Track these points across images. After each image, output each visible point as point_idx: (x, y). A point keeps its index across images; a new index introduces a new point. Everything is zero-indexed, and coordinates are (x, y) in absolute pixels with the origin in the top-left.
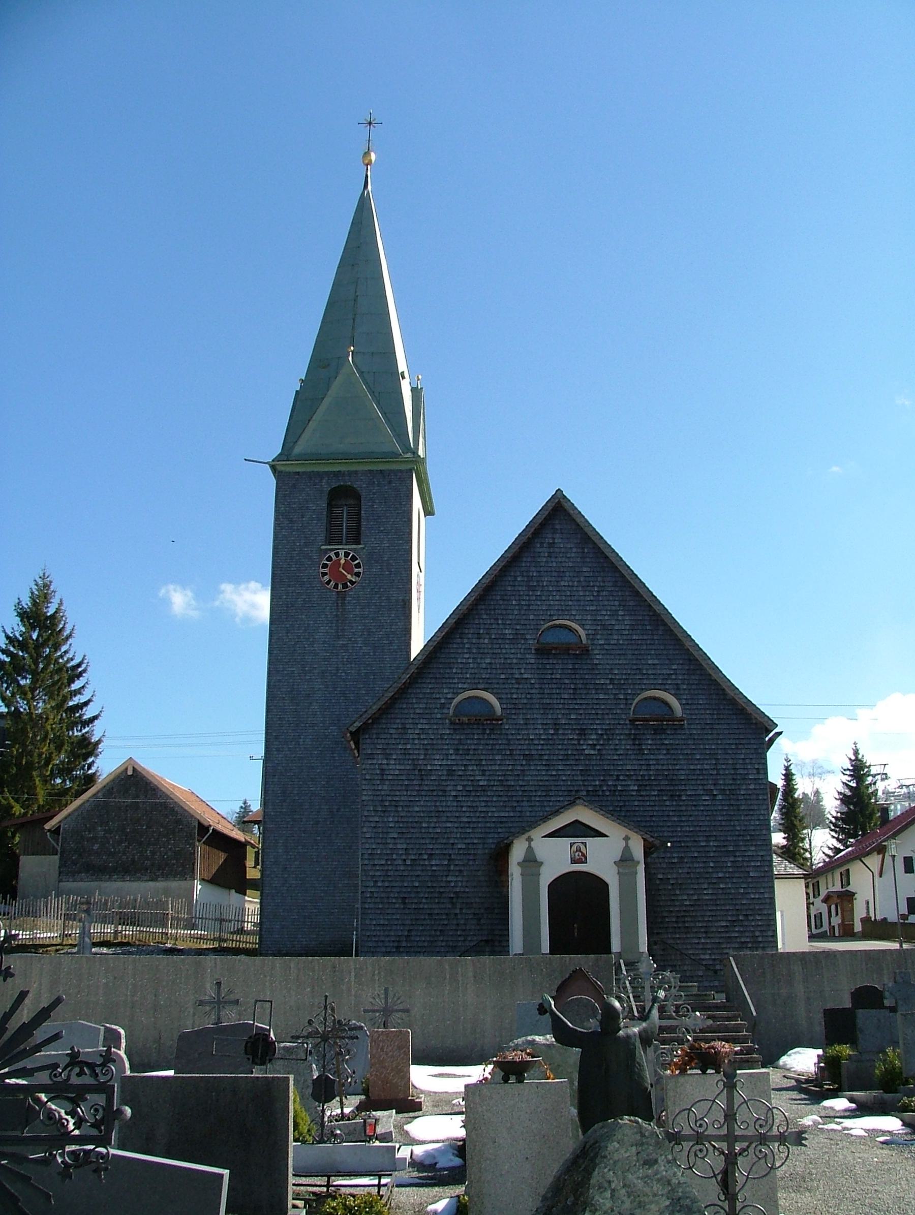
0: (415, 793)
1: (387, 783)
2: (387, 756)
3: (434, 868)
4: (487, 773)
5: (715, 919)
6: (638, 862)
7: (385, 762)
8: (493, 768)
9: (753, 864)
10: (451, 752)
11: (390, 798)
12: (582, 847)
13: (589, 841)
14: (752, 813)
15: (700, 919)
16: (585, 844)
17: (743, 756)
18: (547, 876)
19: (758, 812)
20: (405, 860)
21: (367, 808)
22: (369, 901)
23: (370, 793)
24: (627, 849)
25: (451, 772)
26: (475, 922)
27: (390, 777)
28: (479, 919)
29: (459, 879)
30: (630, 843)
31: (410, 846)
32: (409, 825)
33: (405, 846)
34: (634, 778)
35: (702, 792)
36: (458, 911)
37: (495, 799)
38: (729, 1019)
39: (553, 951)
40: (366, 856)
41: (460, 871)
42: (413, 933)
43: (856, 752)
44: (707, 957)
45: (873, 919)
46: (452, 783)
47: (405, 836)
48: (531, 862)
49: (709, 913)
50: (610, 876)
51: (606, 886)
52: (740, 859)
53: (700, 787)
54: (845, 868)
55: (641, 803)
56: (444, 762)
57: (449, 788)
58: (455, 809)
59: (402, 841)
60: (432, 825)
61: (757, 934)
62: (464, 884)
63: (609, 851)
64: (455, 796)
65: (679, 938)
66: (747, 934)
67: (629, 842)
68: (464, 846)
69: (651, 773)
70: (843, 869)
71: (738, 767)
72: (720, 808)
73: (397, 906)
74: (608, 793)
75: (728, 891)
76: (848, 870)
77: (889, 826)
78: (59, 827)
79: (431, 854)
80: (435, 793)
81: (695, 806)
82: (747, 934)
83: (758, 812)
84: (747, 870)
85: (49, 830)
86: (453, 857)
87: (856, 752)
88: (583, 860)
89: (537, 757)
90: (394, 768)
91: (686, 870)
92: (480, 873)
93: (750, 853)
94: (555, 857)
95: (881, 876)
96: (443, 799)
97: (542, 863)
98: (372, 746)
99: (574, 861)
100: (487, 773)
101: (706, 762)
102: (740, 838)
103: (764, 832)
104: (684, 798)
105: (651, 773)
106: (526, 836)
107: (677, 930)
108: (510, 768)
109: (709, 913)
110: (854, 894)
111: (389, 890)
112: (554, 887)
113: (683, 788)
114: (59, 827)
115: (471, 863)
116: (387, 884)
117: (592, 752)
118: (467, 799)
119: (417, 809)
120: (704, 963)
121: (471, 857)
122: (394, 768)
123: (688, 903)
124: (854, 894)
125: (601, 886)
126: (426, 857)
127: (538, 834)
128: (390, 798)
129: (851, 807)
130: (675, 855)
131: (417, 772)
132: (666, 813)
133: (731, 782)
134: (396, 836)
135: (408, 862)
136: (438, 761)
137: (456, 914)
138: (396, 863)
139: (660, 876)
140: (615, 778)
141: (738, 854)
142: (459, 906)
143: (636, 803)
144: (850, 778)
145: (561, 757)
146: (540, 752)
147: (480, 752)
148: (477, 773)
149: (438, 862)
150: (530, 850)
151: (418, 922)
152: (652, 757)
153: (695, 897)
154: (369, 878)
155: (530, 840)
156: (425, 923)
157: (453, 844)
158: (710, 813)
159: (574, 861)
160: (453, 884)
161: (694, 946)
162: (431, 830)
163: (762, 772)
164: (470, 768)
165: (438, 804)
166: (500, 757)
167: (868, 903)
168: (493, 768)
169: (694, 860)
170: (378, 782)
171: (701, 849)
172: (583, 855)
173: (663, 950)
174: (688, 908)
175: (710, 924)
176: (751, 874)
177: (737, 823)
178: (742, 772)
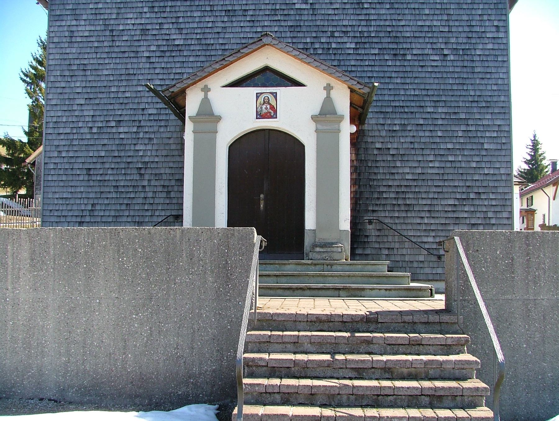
0: (105, 56)
1: (76, 45)
2: (76, 17)
3: (122, 136)
4: (184, 31)
5: (441, 196)
6: (342, 117)
7: (74, 23)
8: (191, 25)
9: (488, 134)
10: (146, 10)
11: (78, 62)
12: (271, 98)
13: (281, 91)
14: (488, 76)
15: (424, 196)
16: (275, 95)
17: (480, 12)
18: (227, 135)
19: (496, 76)
20: (91, 128)
21: (55, 73)
22: (52, 172)
23: (58, 57)
24: (328, 101)
25: (144, 31)
26: (164, 195)
27: (79, 39)
28: (169, 192)
29: (149, 147)
30: (333, 94)
31: (98, 113)
32: (98, 90)
33: (92, 113)
34: (351, 34)
35: (430, 52)
36: (145, 183)
37: (191, 59)
38: (448, 349)
39: (230, 223)
40: (51, 125)
41: (150, 139)
42: (98, 207)
43: (535, 137)
44: (430, 239)
45: (547, 225)
46: (146, 43)
47: (92, 102)
48: (209, 117)
49: (434, 190)
50: (307, 136)
51: (302, 147)
52: (473, 128)
53: (429, 46)
54: (530, 195)
55: (359, 63)
56: (138, 21)
57: (143, 49)
58: (147, 71)
59: (89, 107)
60: (122, 89)
61: (490, 215)
62: (154, 153)
63: (308, 106)
64: (149, 57)
65: (398, 217)
66: (478, 215)
67: (332, 92)
68: (155, 112)
69: (372, 29)
70: (529, 196)
71: (474, 23)
72: (451, 70)
73: (81, 178)
74: (320, 52)
75: (458, 165)
76: (532, 196)
77: (556, 172)
78: (35, 162)
79: (120, 121)
80: (126, 55)
81: (422, 66)
82: (478, 215)
83: (496, 76)
84: (481, 141)
85: (29, 163)
86: (143, 124)
87: (535, 137)
88: (272, 113)
89: (240, 13)
90: (84, 29)
91: (409, 140)
92: (171, 141)
93: (485, 122)
94: (230, 109)
95: (554, 200)
96: (135, 60)
97: (219, 118)
98: (61, 7)
99: (260, 116)
100: (184, 31)
101: (436, 18)
102: (474, 105)
103: (502, 98)
104: (409, 57)
105: (372, 29)
106: (201, 85)
107: (396, 208)
108: (210, 25)
109: (434, 190)
110: (535, 211)
111: (73, 160)
112: (234, 148)
113: (408, 46)
114: (35, 162)
115: (162, 130)
116: (71, 154)
117: (304, 6)
118: (161, 60)
119: (106, 72)
120: (427, 246)
121: (163, 124)
122: (84, 29)
123: (409, 177)
124: (535, 211)
125: (298, 148)
126: (113, 124)
127: (217, 83)
128: (78, 62)
129: (530, 166)
130: (396, 122)
131: (108, 33)
132: (388, 75)
133: (465, 41)
134: (83, 102)
135: (95, 130)
136: (131, 20)
137: (144, 187)
138: (82, 131)
139: (378, 146)
140: (329, 34)
141: (470, 122)
142: (147, 177)
143: (353, 63)
144: (530, 150)
145: (267, 13)
146: (244, 8)
147: (177, 9)
148: (173, 31)
149: (126, 130)
150: (206, 103)
151: (103, 196)
152: (373, 12)
153: (419, 171)
154: (53, 148)
155: (206, 90)
156: (110, 196)
157: (143, 109)
158: (438, 75)
159: (260, 116)
160: (141, 153)
161: (415, 227)
162: (120, 95)
163: (502, 29)
164: (166, 26)
165: (129, 66)
166: (199, 14)
167: (544, 215)
168: (191, 25)
169: (419, 128)
170: (66, 45)
171: (428, 116)
172: (272, 107)
173: (379, 230)
174: (411, 183)
175: (435, 202)
176: (486, 146)
177: (470, 87)
178: (478, 29)
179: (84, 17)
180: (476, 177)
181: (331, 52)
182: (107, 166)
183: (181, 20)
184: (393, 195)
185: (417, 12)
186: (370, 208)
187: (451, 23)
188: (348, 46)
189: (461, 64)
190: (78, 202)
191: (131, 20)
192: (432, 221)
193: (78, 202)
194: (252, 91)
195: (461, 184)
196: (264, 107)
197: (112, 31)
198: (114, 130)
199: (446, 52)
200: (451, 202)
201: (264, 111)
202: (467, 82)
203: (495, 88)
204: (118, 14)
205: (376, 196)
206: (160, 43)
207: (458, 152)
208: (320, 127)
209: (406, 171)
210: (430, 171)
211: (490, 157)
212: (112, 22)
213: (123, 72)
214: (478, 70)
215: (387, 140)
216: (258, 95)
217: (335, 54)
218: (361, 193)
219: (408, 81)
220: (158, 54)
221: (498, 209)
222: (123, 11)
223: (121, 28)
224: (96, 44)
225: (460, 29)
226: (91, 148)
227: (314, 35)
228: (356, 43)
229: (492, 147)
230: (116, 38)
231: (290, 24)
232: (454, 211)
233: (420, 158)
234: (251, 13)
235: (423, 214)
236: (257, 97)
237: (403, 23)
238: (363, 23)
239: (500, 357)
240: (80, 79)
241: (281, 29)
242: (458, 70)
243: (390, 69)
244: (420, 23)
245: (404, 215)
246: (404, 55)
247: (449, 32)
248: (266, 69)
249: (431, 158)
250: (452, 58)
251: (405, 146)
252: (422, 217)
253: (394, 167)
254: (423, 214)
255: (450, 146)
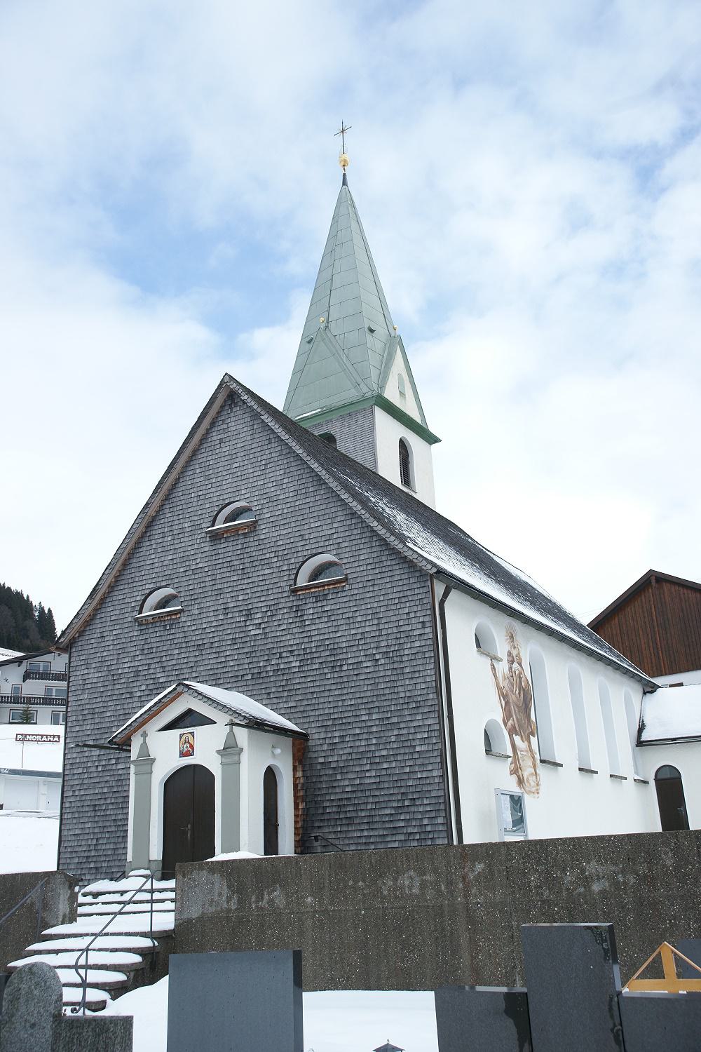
1: (87, 691)
3: (120, 772)
7: (86, 672)
10: (138, 653)
12: (190, 736)
13: (198, 730)
16: (192, 734)
27: (89, 686)
34: (296, 653)
48: (147, 761)
49: (371, 800)
55: (303, 680)
64: (140, 696)
75: (392, 772)
93: (416, 724)
94: (164, 752)
99: (182, 755)
100: (167, 669)
102: (405, 706)
106: (140, 731)
109: (371, 800)
113: (344, 656)
119: (108, 714)
126: (113, 761)
128: (88, 707)
131: (110, 678)
132: (328, 688)
139: (321, 760)
141: (402, 725)
145: (229, 642)
148: (158, 670)
150: (144, 746)
151: (106, 830)
156: (110, 830)
171: (363, 725)
176: (418, 749)
179: (93, 666)
180: (410, 783)
181: (279, 673)
182: (108, 801)
183: (164, 659)
184: (335, 809)
185: (351, 621)
186: (316, 825)
187: (382, 627)
188: (294, 664)
189: (391, 666)
190: (86, 837)
191: (127, 665)
192: (372, 833)
193: (86, 837)
194: (176, 733)
195: (396, 791)
196: (185, 746)
197: (113, 675)
198: (114, 767)
199: (377, 657)
200: (388, 811)
201: (185, 750)
202: (398, 683)
203: (423, 686)
204: (118, 659)
205: (320, 811)
206: (148, 682)
207: (392, 759)
208: (224, 760)
209: (346, 784)
210: (367, 781)
211: (422, 760)
212: (113, 667)
213: (121, 712)
214: (407, 670)
215: (329, 753)
216: (181, 736)
217: (283, 674)
218: (308, 809)
219: (345, 691)
220: (147, 693)
221: (433, 814)
222: (121, 656)
223: (120, 672)
224: (102, 689)
225: (389, 632)
226: (98, 785)
227: (266, 658)
228: (301, 661)
229: (424, 748)
230: (116, 682)
231: (247, 650)
232: (391, 821)
233: (358, 769)
234: (216, 645)
235: (362, 827)
236: (181, 738)
237: (339, 635)
238: (306, 640)
239: (667, 992)
240: (90, 722)
241: (240, 657)
242: (389, 673)
243: (329, 682)
244: (353, 632)
245: (345, 829)
246: (341, 666)
247: (379, 636)
248: (190, 712)
249: (368, 767)
250: (383, 661)
251: (344, 758)
252: (362, 830)
253: (335, 780)
254: (362, 827)
255: (384, 753)
